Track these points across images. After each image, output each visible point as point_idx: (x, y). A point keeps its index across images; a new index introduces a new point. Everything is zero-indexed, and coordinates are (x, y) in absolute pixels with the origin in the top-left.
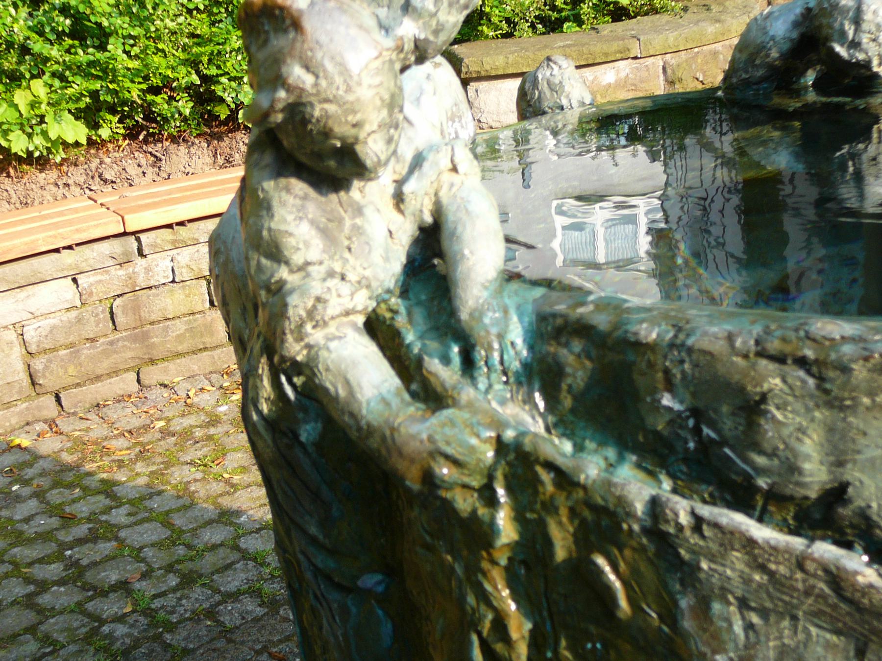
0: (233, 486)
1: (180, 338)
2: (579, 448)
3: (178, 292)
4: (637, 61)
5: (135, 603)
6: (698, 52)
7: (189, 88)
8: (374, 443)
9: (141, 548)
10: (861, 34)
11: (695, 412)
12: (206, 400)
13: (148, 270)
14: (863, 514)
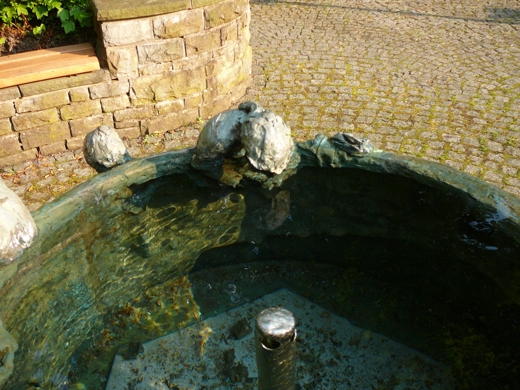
4: (190, 10)
6: (222, 4)
10: (265, 156)
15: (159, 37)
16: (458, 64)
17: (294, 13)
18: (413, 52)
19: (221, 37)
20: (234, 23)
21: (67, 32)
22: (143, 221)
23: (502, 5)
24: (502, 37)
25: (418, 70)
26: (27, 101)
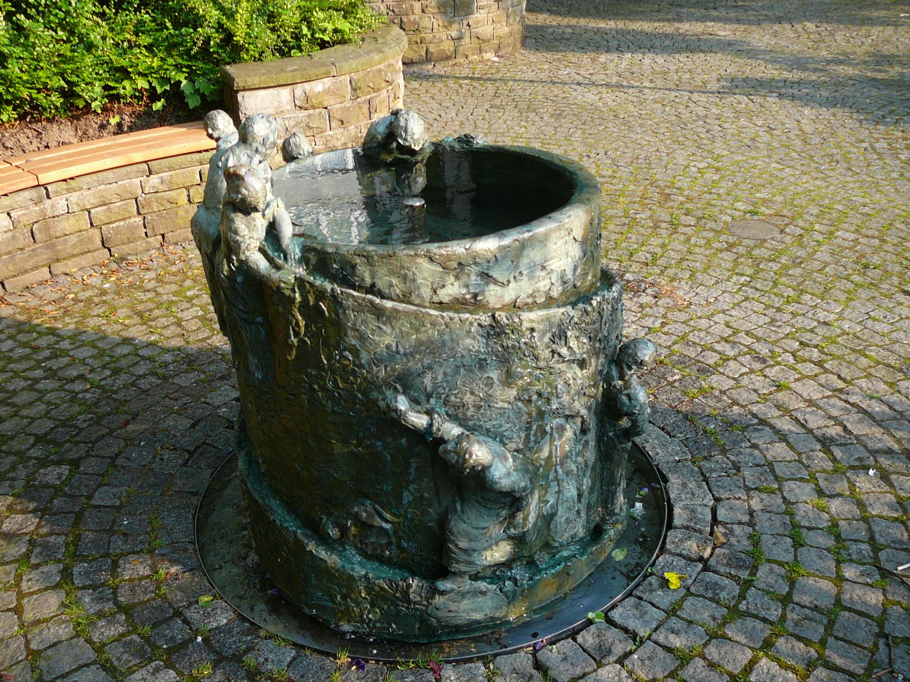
0: (126, 326)
1: (74, 246)
2: (315, 278)
3: (72, 220)
5: (91, 383)
8: (265, 279)
9: (84, 359)
11: (341, 268)
12: (96, 280)
13: (53, 206)
14: (379, 289)
15: (301, 108)
16: (669, 142)
17: (464, 90)
18: (615, 130)
20: (384, 93)
21: (191, 106)
23: (743, 73)
24: (733, 111)
25: (616, 150)
26: (154, 180)
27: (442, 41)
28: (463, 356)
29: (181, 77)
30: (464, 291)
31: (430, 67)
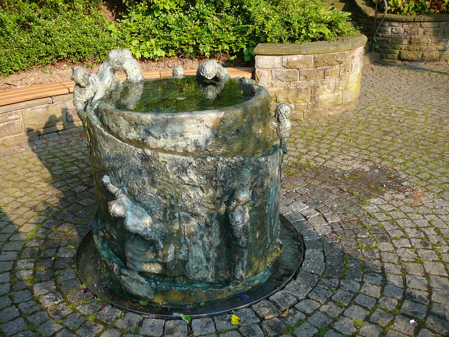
7: (193, 46)
19: (324, 73)
22: (300, 220)
27: (432, 51)
28: (132, 166)
29: (244, 47)
30: (138, 136)
31: (423, 64)
